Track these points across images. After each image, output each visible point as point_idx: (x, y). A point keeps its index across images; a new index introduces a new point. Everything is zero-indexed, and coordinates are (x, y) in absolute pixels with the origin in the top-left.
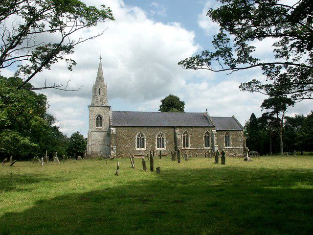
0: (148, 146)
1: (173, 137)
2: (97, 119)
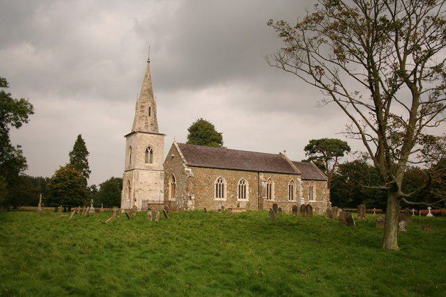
0: (228, 195)
1: (256, 184)
2: (147, 151)
